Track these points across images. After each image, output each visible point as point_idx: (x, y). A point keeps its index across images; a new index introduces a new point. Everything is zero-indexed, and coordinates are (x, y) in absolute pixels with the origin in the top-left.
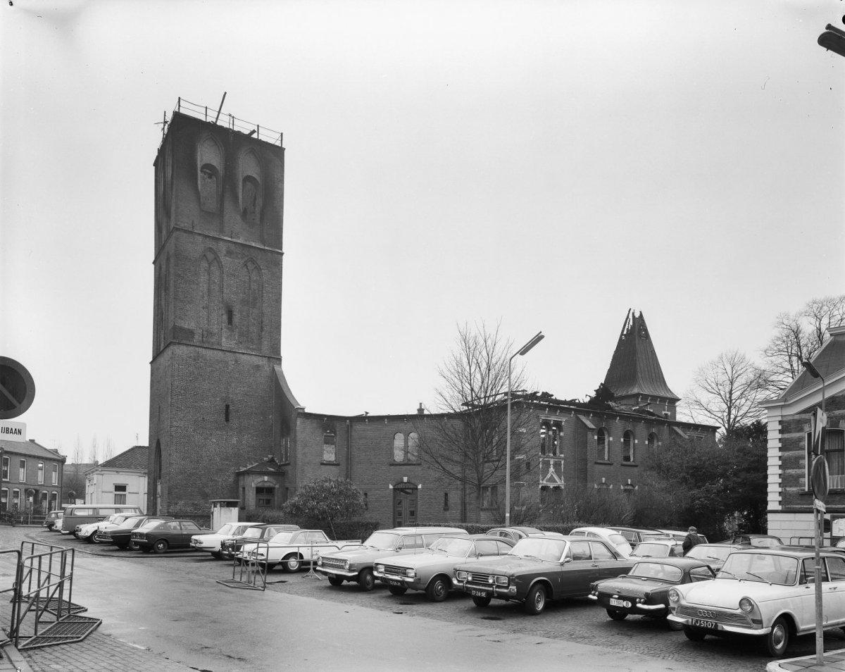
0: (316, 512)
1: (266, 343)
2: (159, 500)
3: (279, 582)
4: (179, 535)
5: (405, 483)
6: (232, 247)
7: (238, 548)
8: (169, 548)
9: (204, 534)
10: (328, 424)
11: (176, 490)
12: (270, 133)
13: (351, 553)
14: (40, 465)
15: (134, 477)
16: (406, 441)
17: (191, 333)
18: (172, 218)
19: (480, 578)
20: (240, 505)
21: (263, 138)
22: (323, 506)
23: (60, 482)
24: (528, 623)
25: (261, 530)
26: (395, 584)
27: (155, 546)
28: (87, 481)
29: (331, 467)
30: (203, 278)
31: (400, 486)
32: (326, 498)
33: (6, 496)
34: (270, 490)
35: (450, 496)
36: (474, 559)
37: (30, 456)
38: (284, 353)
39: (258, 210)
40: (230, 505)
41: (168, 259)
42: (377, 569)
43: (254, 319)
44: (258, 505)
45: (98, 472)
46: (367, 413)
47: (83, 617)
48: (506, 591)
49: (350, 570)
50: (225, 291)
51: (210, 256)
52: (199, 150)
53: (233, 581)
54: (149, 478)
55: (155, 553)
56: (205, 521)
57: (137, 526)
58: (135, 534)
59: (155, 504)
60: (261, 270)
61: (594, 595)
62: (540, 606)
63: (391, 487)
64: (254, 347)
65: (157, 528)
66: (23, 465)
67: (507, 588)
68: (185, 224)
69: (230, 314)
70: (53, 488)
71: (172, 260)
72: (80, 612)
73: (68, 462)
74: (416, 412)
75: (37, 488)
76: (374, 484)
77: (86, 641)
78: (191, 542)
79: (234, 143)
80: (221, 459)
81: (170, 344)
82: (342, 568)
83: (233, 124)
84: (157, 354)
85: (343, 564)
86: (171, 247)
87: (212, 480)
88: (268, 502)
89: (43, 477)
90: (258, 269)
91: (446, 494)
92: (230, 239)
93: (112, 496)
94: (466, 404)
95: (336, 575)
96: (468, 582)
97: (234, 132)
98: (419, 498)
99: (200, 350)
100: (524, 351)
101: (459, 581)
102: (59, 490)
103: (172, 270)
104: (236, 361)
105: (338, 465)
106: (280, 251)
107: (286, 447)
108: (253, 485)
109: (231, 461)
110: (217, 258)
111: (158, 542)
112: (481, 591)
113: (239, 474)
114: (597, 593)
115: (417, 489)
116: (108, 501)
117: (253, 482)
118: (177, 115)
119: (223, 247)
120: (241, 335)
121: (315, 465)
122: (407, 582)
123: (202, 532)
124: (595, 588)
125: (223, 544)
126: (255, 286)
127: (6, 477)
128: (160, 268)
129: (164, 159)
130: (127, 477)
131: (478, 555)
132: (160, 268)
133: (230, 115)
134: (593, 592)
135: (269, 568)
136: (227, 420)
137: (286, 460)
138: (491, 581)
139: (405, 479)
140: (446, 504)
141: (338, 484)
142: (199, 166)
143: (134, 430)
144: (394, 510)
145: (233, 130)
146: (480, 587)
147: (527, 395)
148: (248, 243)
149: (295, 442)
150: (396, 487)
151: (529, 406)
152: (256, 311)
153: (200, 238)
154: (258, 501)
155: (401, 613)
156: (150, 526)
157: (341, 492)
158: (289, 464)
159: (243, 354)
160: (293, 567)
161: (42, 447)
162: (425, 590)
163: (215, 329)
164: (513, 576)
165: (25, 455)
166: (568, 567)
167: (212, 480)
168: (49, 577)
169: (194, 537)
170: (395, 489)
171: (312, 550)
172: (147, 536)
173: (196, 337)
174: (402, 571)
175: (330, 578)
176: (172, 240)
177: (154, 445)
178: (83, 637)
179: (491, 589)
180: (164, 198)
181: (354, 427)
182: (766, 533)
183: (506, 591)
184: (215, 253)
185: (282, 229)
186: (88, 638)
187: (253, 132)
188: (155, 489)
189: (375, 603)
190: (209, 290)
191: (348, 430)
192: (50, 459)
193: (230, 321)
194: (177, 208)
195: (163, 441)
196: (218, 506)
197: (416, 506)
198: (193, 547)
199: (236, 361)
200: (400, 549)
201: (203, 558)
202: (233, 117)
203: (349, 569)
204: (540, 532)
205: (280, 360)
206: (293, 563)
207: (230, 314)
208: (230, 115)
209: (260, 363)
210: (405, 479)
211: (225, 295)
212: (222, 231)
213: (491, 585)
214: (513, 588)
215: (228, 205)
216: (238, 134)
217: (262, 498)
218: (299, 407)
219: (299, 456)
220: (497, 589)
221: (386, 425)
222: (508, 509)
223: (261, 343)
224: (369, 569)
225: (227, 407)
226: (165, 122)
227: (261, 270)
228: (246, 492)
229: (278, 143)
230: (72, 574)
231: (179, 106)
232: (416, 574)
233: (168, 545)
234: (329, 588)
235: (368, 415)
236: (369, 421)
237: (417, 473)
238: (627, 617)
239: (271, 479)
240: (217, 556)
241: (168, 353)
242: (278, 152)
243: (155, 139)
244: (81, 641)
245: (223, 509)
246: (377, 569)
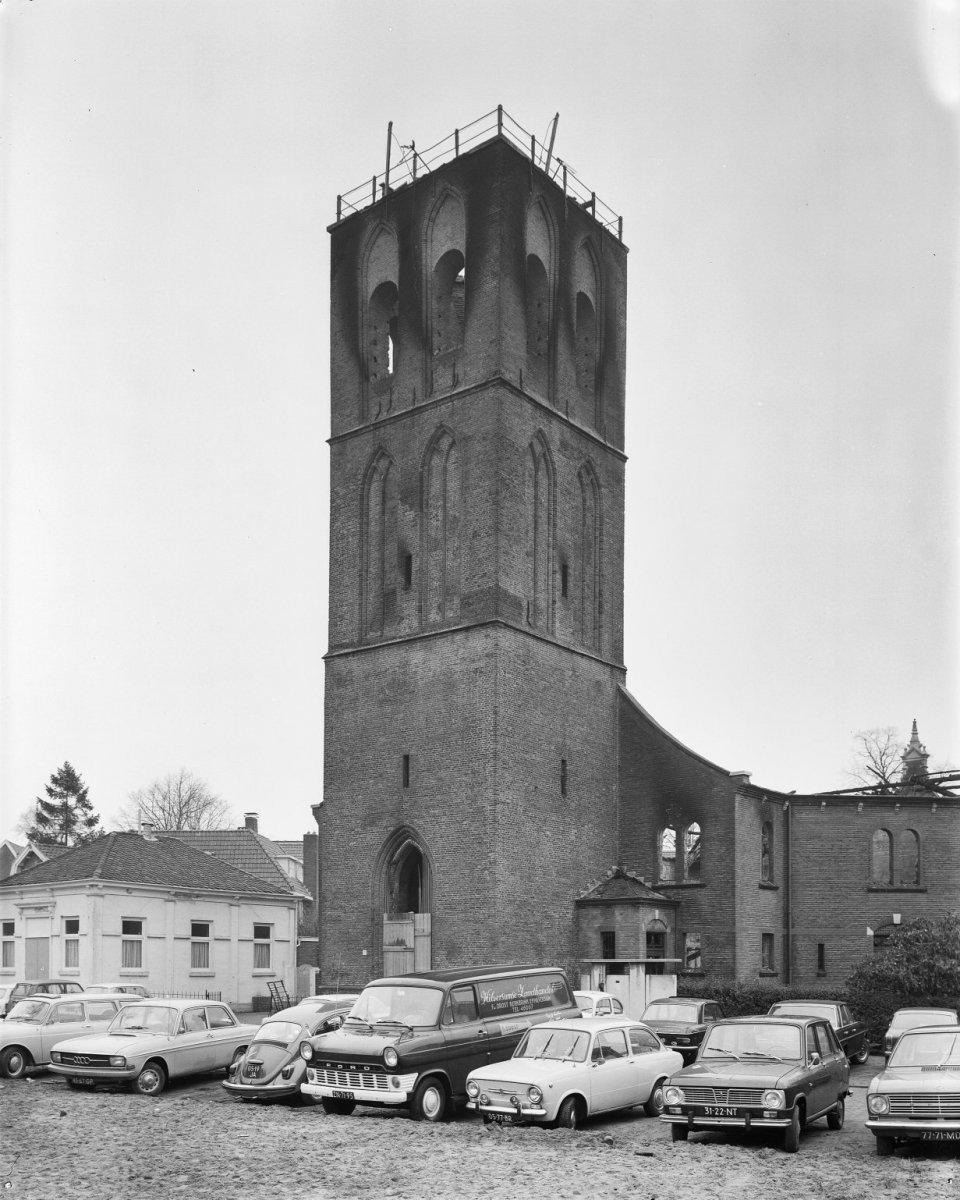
5: (896, 925)
16: (679, 843)
38: (325, 452)
60: (599, 486)
63: (870, 932)
76: (838, 927)
92: (564, 417)
109: (568, 877)
110: (547, 454)
136: (564, 791)
139: (897, 918)
140: (821, 965)
150: (881, 933)
170: (875, 936)
181: (798, 816)
182: (67, 922)
210: (897, 918)
227: (599, 486)
237: (918, 907)
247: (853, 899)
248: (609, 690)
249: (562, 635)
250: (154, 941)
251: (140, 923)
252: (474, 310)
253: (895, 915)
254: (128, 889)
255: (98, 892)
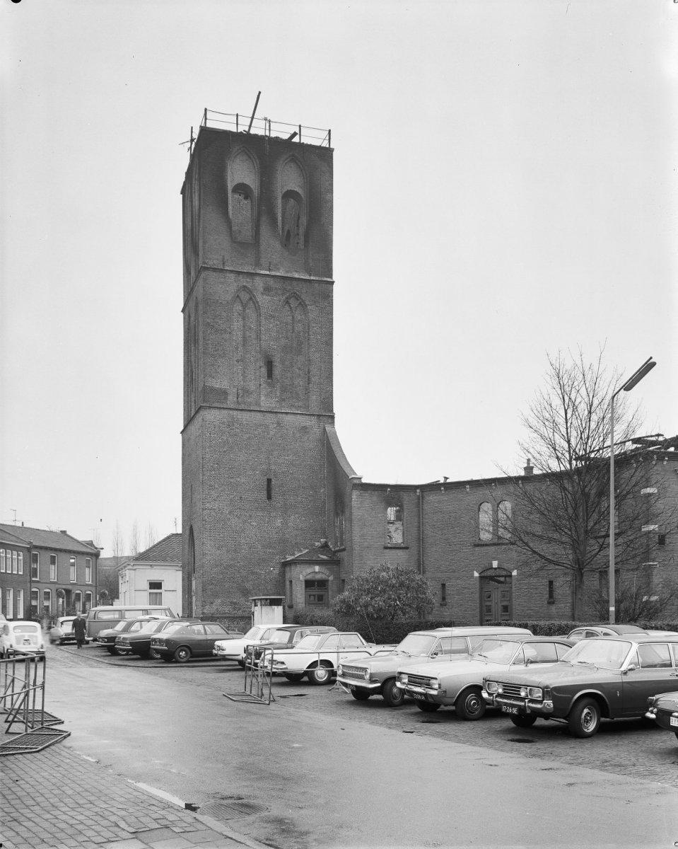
0: (371, 609)
1: (314, 397)
2: (194, 598)
3: (296, 696)
4: (204, 640)
5: (495, 569)
6: (271, 282)
7: (258, 655)
8: (191, 657)
9: (233, 639)
10: (392, 494)
11: (211, 587)
12: (316, 133)
13: (379, 660)
14: (72, 561)
15: (170, 571)
17: (224, 393)
18: (200, 255)
19: (511, 689)
20: (288, 602)
21: (305, 140)
22: (379, 602)
23: (94, 579)
24: (566, 750)
25: (288, 634)
26: (419, 697)
27: (176, 653)
28: (120, 578)
29: (398, 551)
30: (237, 325)
31: (489, 573)
32: (384, 591)
33: (36, 598)
34: (322, 584)
35: (556, 584)
36: (522, 667)
37: (60, 550)
39: (302, 231)
40: (274, 602)
41: (197, 306)
42: (400, 680)
43: (299, 369)
44: (308, 602)
45: (130, 567)
46: (446, 478)
47: (56, 730)
48: (539, 706)
49: (372, 681)
50: (263, 337)
51: (245, 296)
52: (229, 167)
53: (243, 694)
54: (183, 572)
55: (177, 662)
56: (243, 623)
57: (158, 630)
58: (154, 640)
59: (191, 603)
61: (652, 712)
62: (592, 727)
63: (476, 574)
64: (300, 404)
65: (178, 632)
66: (53, 561)
67: (540, 702)
68: (214, 262)
69: (270, 365)
70: (86, 588)
71: (201, 307)
72: (56, 724)
73: (103, 555)
74: (522, 473)
75: (69, 587)
77: (43, 752)
78: (214, 649)
79: (268, 152)
80: (263, 546)
81: (200, 408)
82: (361, 677)
83: (270, 130)
84: (189, 421)
85: (364, 673)
86: (199, 291)
87: (253, 573)
88: (320, 598)
89: (78, 575)
90: (303, 305)
91: (551, 583)
92: (268, 273)
93: (146, 594)
94: (579, 458)
95: (356, 686)
96: (499, 695)
97: (270, 138)
98: (514, 589)
99: (235, 413)
100: (629, 386)
101: (489, 694)
102: (94, 589)
103: (200, 319)
104: (278, 424)
105: (407, 548)
106: (329, 280)
107: (341, 528)
108: (301, 578)
110: (252, 298)
111: (179, 649)
112: (513, 706)
113: (285, 565)
114: (655, 710)
115: (511, 576)
116: (143, 601)
117: (301, 574)
118: (204, 131)
119: (259, 283)
120: (284, 390)
121: (376, 547)
122: (431, 695)
123: (227, 636)
124: (654, 704)
125: (246, 651)
126: (299, 327)
127: (36, 577)
128: (189, 317)
129: (191, 184)
130: (162, 571)
131: (527, 663)
132: (189, 317)
133: (266, 119)
134: (650, 709)
135: (295, 679)
136: (269, 497)
137: (342, 544)
138: (523, 694)
139: (495, 564)
140: (551, 596)
141: (399, 573)
142: (230, 187)
143: (164, 516)
144: (481, 604)
145: (269, 137)
146: (512, 702)
147: (666, 440)
148: (289, 275)
149: (351, 521)
150: (482, 575)
151: (661, 459)
152: (301, 358)
153: (232, 276)
154: (308, 597)
155: (412, 732)
156: (172, 631)
157: (402, 584)
158: (344, 550)
159: (287, 413)
160: (320, 678)
161: (72, 538)
162: (454, 704)
163: (252, 387)
164: (547, 687)
165: (55, 550)
166: (632, 677)
167: (253, 573)
168: (13, 681)
169: (217, 643)
170: (481, 578)
171: (338, 657)
172: (167, 642)
173: (230, 397)
174: (424, 681)
175: (352, 691)
176: (200, 282)
177: (188, 532)
178: (40, 748)
179: (523, 704)
180: (192, 234)
183: (539, 706)
184: (250, 292)
185: (332, 251)
186: (52, 747)
187: (295, 134)
188: (190, 585)
189: (363, 715)
190: (244, 338)
191: (420, 502)
192: (83, 553)
193: (270, 374)
194: (204, 243)
195: (195, 528)
196: (259, 604)
197: (510, 600)
198: (216, 655)
199: (278, 424)
200: (436, 654)
201: (224, 668)
202: (270, 121)
203: (370, 680)
204: (643, 631)
205: (332, 417)
206: (321, 673)
207: (270, 365)
208: (266, 119)
209: (308, 424)
210: (495, 564)
211: (263, 343)
212: (258, 264)
213: (523, 699)
214: (549, 703)
215: (265, 231)
216: (277, 141)
217: (312, 593)
218: (353, 476)
219: (356, 539)
220: (530, 705)
221: (467, 493)
222: (612, 601)
223: (307, 399)
224: (391, 679)
225: (269, 481)
226: (192, 140)
228: (294, 586)
229: (325, 144)
230: (44, 682)
231: (206, 119)
232: (439, 685)
233: (191, 652)
234: (351, 703)
235: (448, 481)
236: (446, 489)
238: (370, 698)
239: (324, 569)
240: (242, 666)
241: (199, 419)
242: (325, 154)
243: (182, 161)
244: (38, 751)
245: (264, 608)
246: (400, 680)
247: (464, 552)
248: (316, 431)
249: (265, 403)
250: (169, 592)
251: (161, 583)
252: (259, 210)
253: (494, 562)
254: (151, 565)
255: (131, 567)
